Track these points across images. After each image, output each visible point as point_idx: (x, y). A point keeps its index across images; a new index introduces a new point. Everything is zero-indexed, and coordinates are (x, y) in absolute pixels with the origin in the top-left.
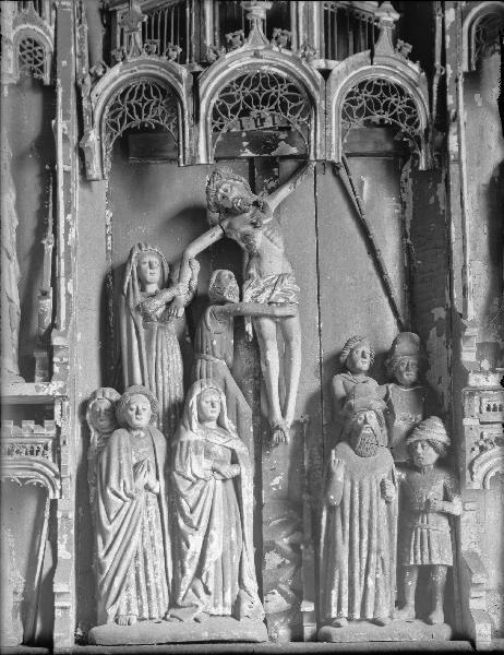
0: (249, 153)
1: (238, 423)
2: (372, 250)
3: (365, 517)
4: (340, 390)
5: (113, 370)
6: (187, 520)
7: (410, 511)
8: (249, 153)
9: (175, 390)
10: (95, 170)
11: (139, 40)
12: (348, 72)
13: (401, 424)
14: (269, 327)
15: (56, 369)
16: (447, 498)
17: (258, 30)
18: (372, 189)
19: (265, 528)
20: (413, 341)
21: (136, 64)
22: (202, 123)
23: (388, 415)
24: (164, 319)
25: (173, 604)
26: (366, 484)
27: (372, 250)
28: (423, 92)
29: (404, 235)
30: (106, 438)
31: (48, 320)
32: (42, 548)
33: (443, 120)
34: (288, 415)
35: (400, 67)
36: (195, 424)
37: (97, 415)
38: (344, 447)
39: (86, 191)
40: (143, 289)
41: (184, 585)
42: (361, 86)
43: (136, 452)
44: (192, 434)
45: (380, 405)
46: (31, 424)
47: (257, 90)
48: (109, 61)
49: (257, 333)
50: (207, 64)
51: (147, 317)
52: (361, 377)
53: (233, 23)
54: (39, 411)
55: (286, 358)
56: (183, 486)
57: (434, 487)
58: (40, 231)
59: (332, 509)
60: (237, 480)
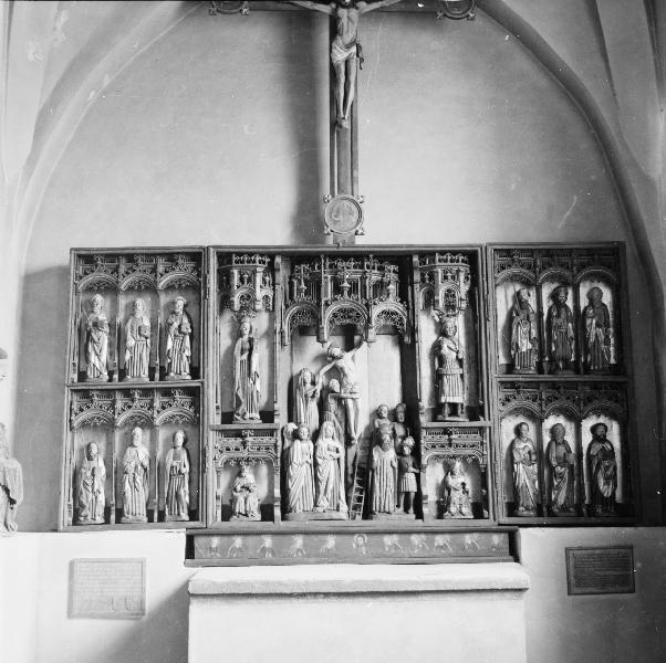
23: (394, 435)
32: (612, 354)
45: (390, 432)
56: (320, 461)
60: (338, 459)
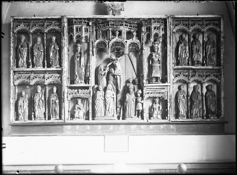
0: (116, 51)
1: (114, 90)
2: (133, 65)
3: (130, 103)
4: (128, 86)
5: (97, 82)
6: (107, 103)
7: (137, 102)
8: (116, 51)
9: (105, 85)
10: (95, 54)
11: (101, 36)
12: (129, 42)
13: (136, 91)
14: (118, 77)
15: (90, 82)
16: (141, 101)
17: (117, 36)
18: (133, 57)
19: (117, 105)
20: (138, 79)
21: (101, 39)
22: (109, 48)
23: (134, 89)
24: (104, 75)
25: (105, 115)
26: (131, 99)
27: (133, 65)
28: (140, 44)
29: (137, 63)
30: (96, 92)
31: (88, 76)
33: (142, 49)
34: (121, 90)
35: (137, 41)
36: (108, 90)
37: (95, 89)
38: (128, 94)
39: (93, 57)
40: (101, 71)
41: (107, 111)
42: (131, 43)
43: (100, 94)
44: (108, 91)
45: (133, 88)
46: (86, 90)
47: (117, 43)
48: (97, 39)
49: (117, 78)
50: (110, 40)
51: (102, 75)
52: (131, 84)
53: (114, 34)
54: (87, 88)
55: (120, 80)
56: (106, 98)
57: (140, 99)
58: (87, 63)
59: (126, 102)
60: (113, 98)
